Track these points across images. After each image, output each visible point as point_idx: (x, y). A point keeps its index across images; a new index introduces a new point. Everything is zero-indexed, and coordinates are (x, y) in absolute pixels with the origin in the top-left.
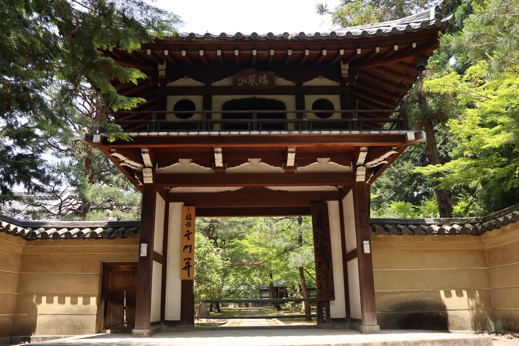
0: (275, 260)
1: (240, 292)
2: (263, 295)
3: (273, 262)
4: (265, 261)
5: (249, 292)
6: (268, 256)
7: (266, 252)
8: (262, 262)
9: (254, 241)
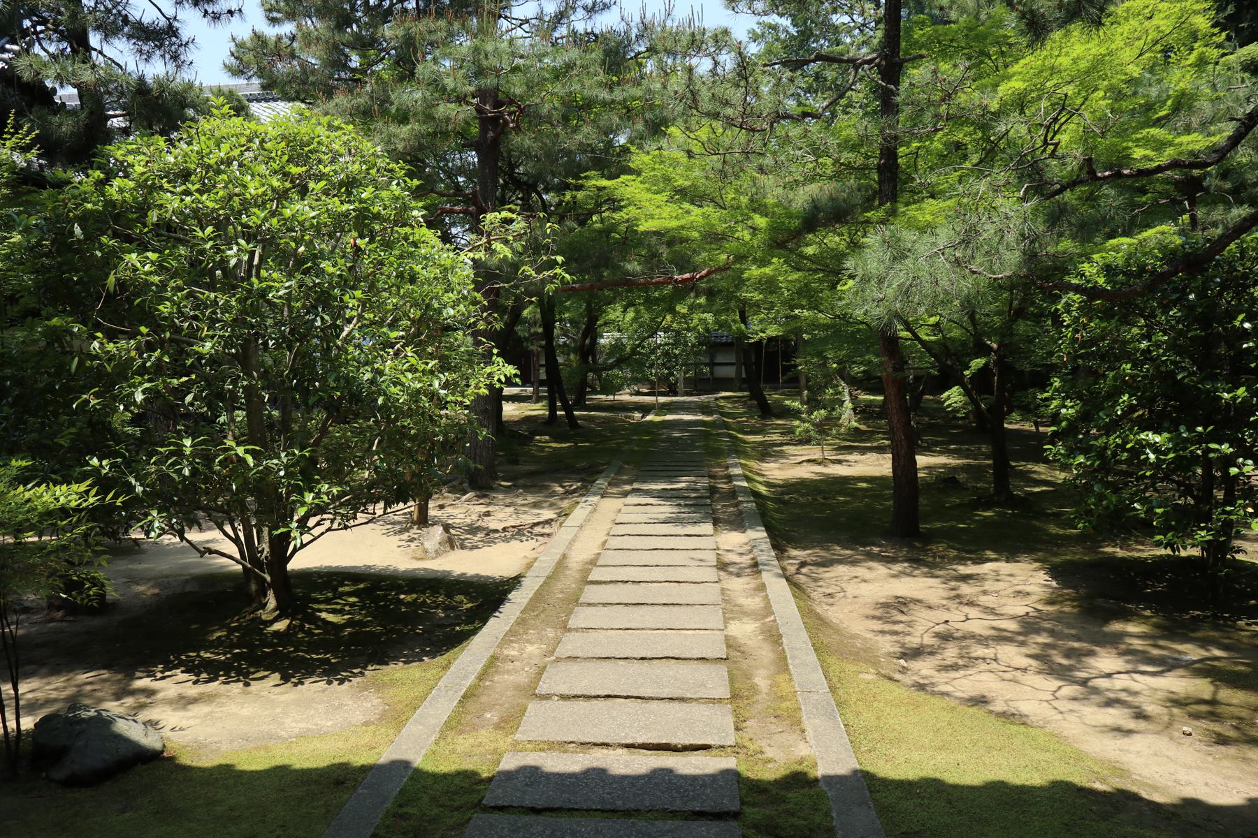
0: (763, 263)
1: (653, 351)
2: (719, 359)
3: (754, 272)
4: (720, 270)
5: (677, 352)
6: (732, 245)
7: (721, 227)
8: (704, 272)
9: (667, 179)
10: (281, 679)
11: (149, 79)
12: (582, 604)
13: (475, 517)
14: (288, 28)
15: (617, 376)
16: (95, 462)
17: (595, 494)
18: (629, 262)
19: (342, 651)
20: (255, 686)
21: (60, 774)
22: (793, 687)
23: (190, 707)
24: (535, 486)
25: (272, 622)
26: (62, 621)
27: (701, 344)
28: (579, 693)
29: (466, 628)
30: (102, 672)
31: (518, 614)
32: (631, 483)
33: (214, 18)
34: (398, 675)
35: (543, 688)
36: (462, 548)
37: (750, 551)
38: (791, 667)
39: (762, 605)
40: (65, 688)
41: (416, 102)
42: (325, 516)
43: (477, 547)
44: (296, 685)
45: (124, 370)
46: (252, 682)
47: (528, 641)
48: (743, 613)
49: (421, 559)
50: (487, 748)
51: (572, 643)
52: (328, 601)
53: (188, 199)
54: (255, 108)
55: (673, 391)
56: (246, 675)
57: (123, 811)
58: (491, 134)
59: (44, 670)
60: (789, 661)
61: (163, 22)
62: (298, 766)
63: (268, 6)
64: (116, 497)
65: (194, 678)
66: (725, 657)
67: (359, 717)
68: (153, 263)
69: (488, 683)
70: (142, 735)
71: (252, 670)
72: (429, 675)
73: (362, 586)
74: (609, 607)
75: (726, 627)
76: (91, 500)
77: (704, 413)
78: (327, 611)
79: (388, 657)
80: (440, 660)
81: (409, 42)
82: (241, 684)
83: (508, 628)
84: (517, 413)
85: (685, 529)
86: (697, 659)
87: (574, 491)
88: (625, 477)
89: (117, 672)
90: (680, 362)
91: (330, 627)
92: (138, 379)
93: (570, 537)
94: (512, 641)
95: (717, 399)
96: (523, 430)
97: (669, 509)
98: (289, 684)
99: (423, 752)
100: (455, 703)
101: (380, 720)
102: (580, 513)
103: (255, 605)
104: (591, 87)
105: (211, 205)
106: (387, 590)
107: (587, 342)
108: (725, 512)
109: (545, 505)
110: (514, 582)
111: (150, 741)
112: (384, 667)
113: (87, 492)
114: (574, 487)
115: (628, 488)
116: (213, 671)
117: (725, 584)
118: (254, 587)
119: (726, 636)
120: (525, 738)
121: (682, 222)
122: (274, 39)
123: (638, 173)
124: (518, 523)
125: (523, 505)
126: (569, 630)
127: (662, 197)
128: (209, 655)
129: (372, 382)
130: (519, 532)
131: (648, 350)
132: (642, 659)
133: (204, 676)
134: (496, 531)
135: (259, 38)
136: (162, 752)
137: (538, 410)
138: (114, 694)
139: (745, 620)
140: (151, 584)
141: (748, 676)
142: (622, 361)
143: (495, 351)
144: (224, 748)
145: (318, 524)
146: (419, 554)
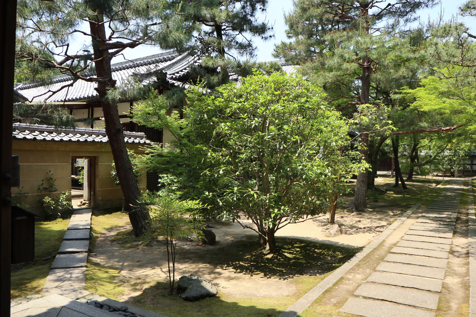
1: (444, 158)
5: (455, 159)
8: (455, 127)
10: (264, 275)
11: (241, 62)
12: (384, 261)
13: (354, 222)
14: (293, 40)
15: (427, 168)
16: (207, 193)
17: (405, 217)
18: (422, 122)
19: (288, 268)
20: (254, 276)
21: (184, 296)
22: (469, 310)
23: (231, 280)
24: (382, 211)
25: (267, 254)
26: (201, 246)
27: (466, 156)
28: (371, 297)
29: (337, 265)
30: (207, 264)
31: (357, 262)
32: (422, 213)
33: (265, 39)
34: (305, 280)
35: (357, 293)
36: (345, 234)
37: (467, 247)
38: (470, 301)
39: (465, 271)
40: (195, 268)
41: (335, 63)
42: (288, 218)
43: (352, 234)
44: (268, 278)
45: (218, 164)
46: (254, 275)
47: (358, 273)
48: (455, 274)
49: (329, 237)
50: (328, 312)
51: (375, 277)
52: (289, 249)
53: (240, 104)
54: (284, 68)
55: (452, 175)
56: (252, 272)
57: (198, 312)
58: (367, 74)
59: (191, 261)
60: (470, 299)
61: (247, 42)
62: (258, 307)
63: (287, 32)
64: (208, 206)
65: (235, 271)
66: (439, 291)
67: (286, 293)
68: (228, 126)
69: (337, 287)
70: (210, 288)
71: (255, 271)
72: (316, 281)
73: (303, 245)
74: (396, 264)
75: (444, 279)
76: (200, 206)
77: (464, 185)
78: (287, 253)
79: (304, 272)
80: (322, 276)
81: (332, 41)
82: (250, 275)
83: (351, 267)
84: (383, 182)
85: (440, 234)
86: (427, 290)
87: (397, 215)
88: (420, 211)
89: (212, 265)
90: (456, 163)
91: (287, 259)
92: (222, 166)
93: (388, 233)
94: (351, 272)
95: (473, 179)
96: (383, 189)
97: (435, 225)
98: (266, 278)
99: (303, 310)
100: (321, 293)
101: (293, 295)
102: (396, 224)
103: (262, 248)
104: (405, 53)
105: (247, 106)
106: (311, 247)
107: (414, 154)
108: (461, 229)
109: (384, 219)
110: (360, 249)
111: (213, 290)
112: (301, 276)
113: (199, 204)
114: (398, 213)
115: (420, 215)
116: (242, 269)
117: (450, 260)
118: (262, 241)
119: (443, 282)
120: (343, 311)
121: (441, 106)
122: (289, 44)
123: (424, 86)
124: (371, 226)
125: (375, 219)
126: (376, 271)
127: (433, 97)
128: (242, 263)
129: (302, 169)
130: (370, 229)
131: (442, 158)
132: (403, 287)
133: (239, 270)
134: (361, 228)
135: (283, 43)
136: (216, 294)
137: (392, 181)
138: (209, 273)
139: (455, 277)
140: (231, 236)
141: (448, 302)
142: (429, 162)
143: (363, 158)
144: (237, 297)
145: (286, 220)
146: (328, 234)
